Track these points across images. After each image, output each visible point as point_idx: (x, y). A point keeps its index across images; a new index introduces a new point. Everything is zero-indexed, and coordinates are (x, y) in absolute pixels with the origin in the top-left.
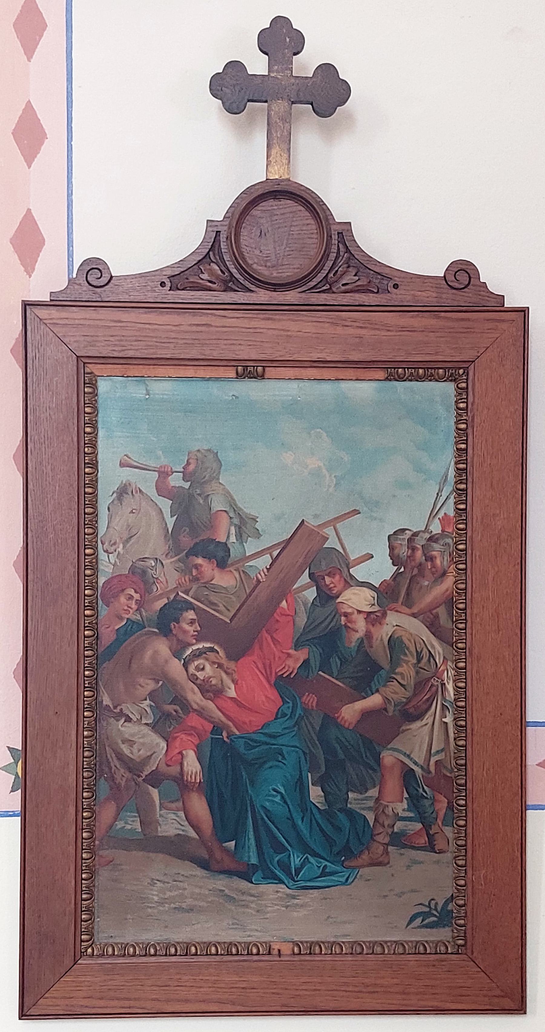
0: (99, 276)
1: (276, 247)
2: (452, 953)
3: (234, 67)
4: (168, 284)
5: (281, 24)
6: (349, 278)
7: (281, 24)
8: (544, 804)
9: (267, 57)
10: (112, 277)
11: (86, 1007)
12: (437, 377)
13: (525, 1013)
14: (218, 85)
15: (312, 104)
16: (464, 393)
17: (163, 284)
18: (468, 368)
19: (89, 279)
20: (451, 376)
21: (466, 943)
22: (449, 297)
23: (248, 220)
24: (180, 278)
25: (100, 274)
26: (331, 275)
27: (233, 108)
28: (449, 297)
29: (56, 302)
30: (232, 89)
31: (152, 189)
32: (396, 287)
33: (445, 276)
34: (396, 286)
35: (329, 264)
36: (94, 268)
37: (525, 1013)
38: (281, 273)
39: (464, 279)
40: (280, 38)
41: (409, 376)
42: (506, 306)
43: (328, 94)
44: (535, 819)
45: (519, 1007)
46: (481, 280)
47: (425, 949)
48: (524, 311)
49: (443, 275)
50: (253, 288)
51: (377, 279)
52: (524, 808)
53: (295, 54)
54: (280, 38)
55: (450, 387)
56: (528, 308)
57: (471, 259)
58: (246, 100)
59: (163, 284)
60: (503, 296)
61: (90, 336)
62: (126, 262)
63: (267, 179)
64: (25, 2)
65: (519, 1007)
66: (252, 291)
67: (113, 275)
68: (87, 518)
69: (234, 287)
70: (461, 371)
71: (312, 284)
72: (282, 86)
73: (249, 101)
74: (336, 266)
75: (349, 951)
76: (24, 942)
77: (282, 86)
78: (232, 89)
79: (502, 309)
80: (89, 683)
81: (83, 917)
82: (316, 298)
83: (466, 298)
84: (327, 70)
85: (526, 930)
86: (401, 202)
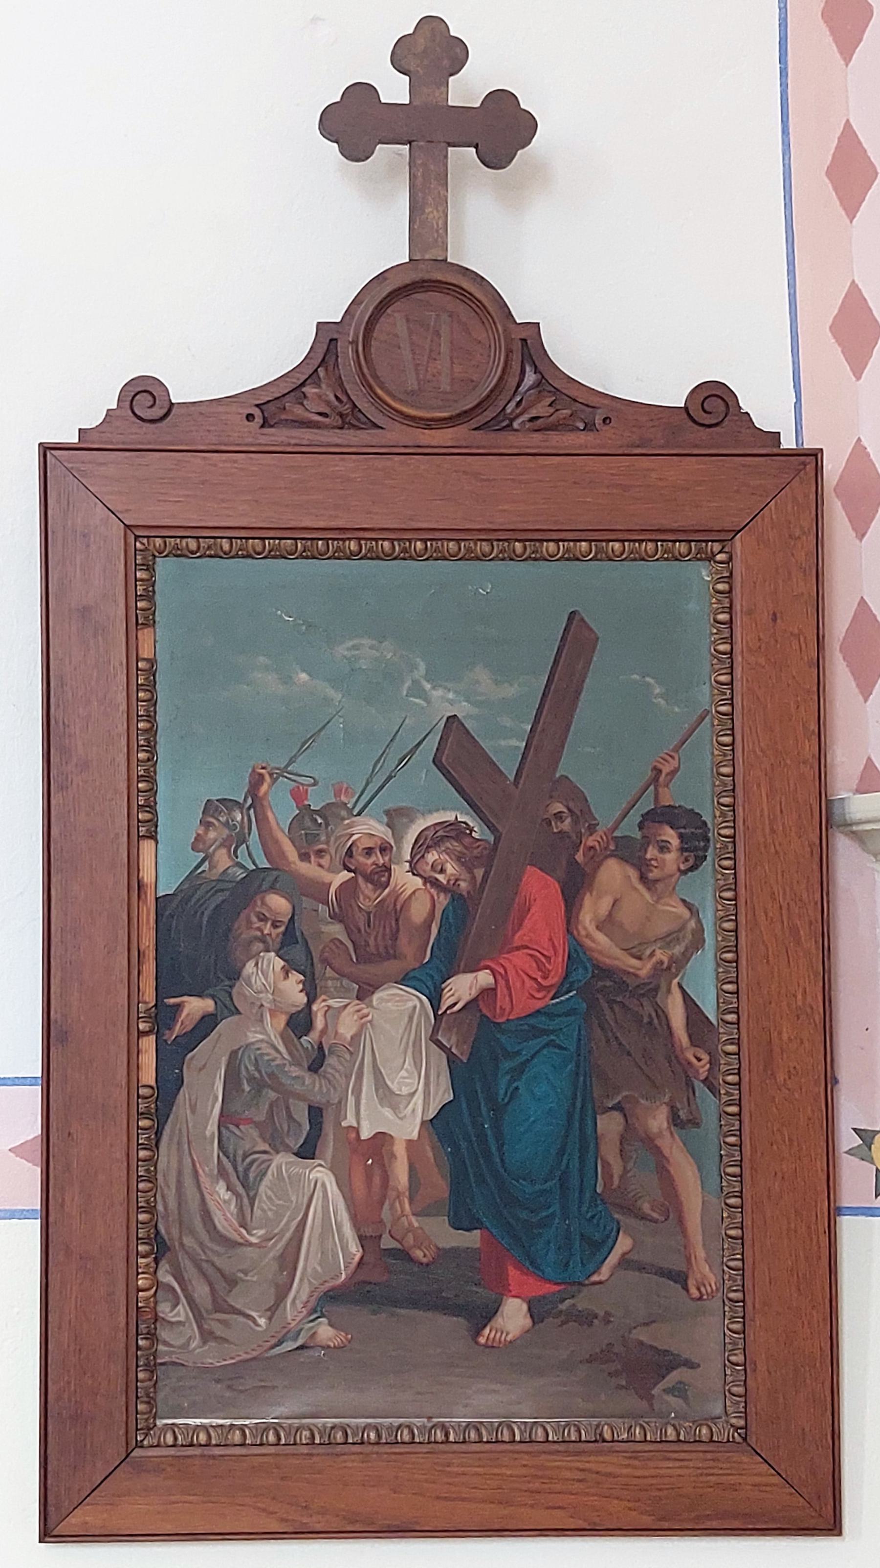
1: (430, 362)
2: (488, 1442)
3: (361, 94)
5: (432, 25)
7: (432, 25)
8: (879, 1206)
10: (172, 404)
12: (447, 554)
13: (840, 1534)
15: (476, 147)
20: (501, 552)
24: (270, 407)
25: (150, 398)
26: (513, 404)
27: (355, 150)
29: (88, 442)
30: (353, 122)
31: (255, 272)
32: (251, 419)
34: (250, 417)
36: (144, 398)
37: (840, 1534)
38: (431, 384)
40: (431, 50)
41: (335, 552)
43: (502, 130)
45: (831, 1525)
47: (480, 1435)
48: (816, 455)
49: (683, 405)
52: (834, 1212)
53: (451, 75)
54: (431, 50)
55: (164, 567)
56: (821, 450)
57: (155, 373)
62: (188, 384)
63: (410, 260)
64: (826, 2)
65: (831, 1525)
66: (376, 426)
67: (173, 401)
69: (354, 422)
71: (489, 414)
72: (432, 120)
75: (358, 1439)
77: (432, 120)
78: (353, 122)
79: (775, 451)
84: (502, 102)
86: (644, 279)
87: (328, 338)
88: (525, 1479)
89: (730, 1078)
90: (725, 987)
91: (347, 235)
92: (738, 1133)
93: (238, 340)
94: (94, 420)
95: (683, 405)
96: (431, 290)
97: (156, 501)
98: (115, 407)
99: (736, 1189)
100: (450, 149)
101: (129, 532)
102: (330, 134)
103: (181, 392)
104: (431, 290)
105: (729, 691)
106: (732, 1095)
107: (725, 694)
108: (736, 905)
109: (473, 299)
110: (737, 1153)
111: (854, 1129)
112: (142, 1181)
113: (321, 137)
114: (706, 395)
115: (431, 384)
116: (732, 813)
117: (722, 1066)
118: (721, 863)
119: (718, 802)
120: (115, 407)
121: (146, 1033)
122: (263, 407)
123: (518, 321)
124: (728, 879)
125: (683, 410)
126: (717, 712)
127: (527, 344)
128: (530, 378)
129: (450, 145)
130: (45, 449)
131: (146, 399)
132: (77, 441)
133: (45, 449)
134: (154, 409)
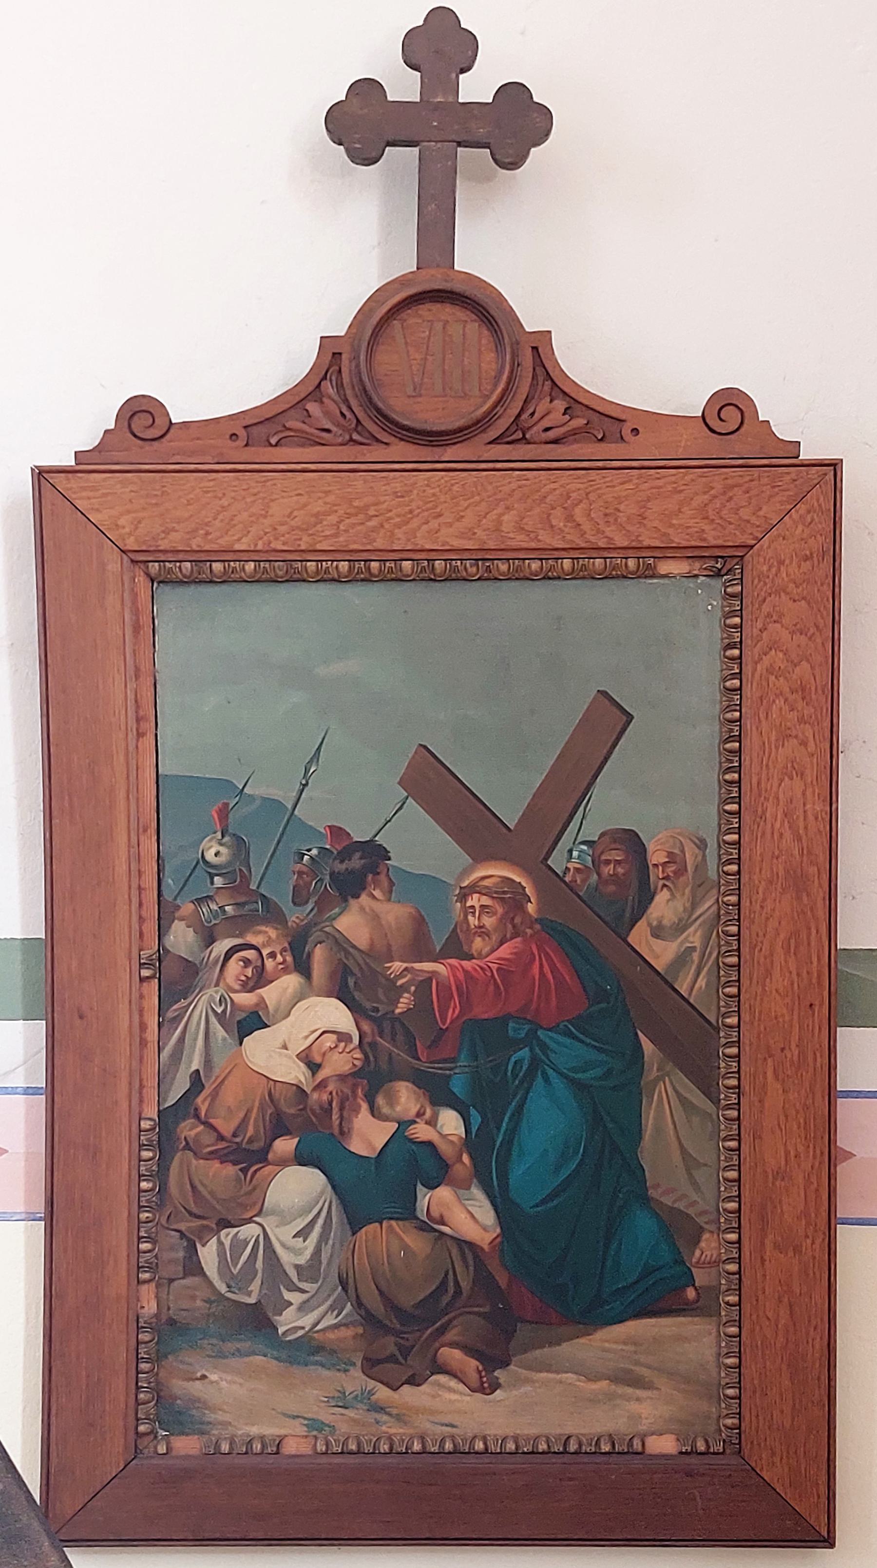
0: (151, 421)
1: (436, 377)
4: (242, 433)
5: (442, 20)
7: (442, 20)
9: (491, 101)
11: (138, 799)
17: (635, 431)
18: (742, 557)
19: (133, 426)
22: (714, 446)
24: (262, 431)
26: (525, 416)
28: (714, 446)
31: (253, 287)
33: (703, 416)
36: (141, 417)
37: (832, 1545)
38: (436, 393)
39: (732, 417)
40: (441, 44)
43: (516, 125)
50: (385, 438)
51: (603, 423)
53: (463, 71)
54: (441, 44)
56: (842, 460)
58: (383, 144)
59: (635, 431)
61: (140, 516)
62: (209, 388)
63: (418, 268)
67: (173, 421)
72: (437, 123)
73: (389, 144)
74: (529, 403)
76: (50, 1341)
77: (437, 123)
78: (361, 125)
83: (738, 446)
84: (514, 94)
86: (627, 293)
87: (331, 352)
89: (729, 1051)
90: (727, 807)
91: (338, 253)
92: (737, 1138)
93: (238, 356)
94: (89, 440)
96: (435, 296)
98: (112, 427)
99: (734, 978)
100: (459, 149)
101: (124, 556)
103: (180, 411)
104: (435, 296)
105: (735, 1064)
106: (731, 854)
109: (480, 306)
110: (736, 1157)
112: (144, 1180)
113: (454, 10)
114: (718, 407)
115: (436, 393)
116: (736, 942)
117: (722, 1039)
122: (249, 429)
123: (527, 330)
127: (533, 357)
129: (459, 144)
130: (41, 475)
131: (147, 420)
132: (73, 463)
133: (41, 475)
134: (151, 430)
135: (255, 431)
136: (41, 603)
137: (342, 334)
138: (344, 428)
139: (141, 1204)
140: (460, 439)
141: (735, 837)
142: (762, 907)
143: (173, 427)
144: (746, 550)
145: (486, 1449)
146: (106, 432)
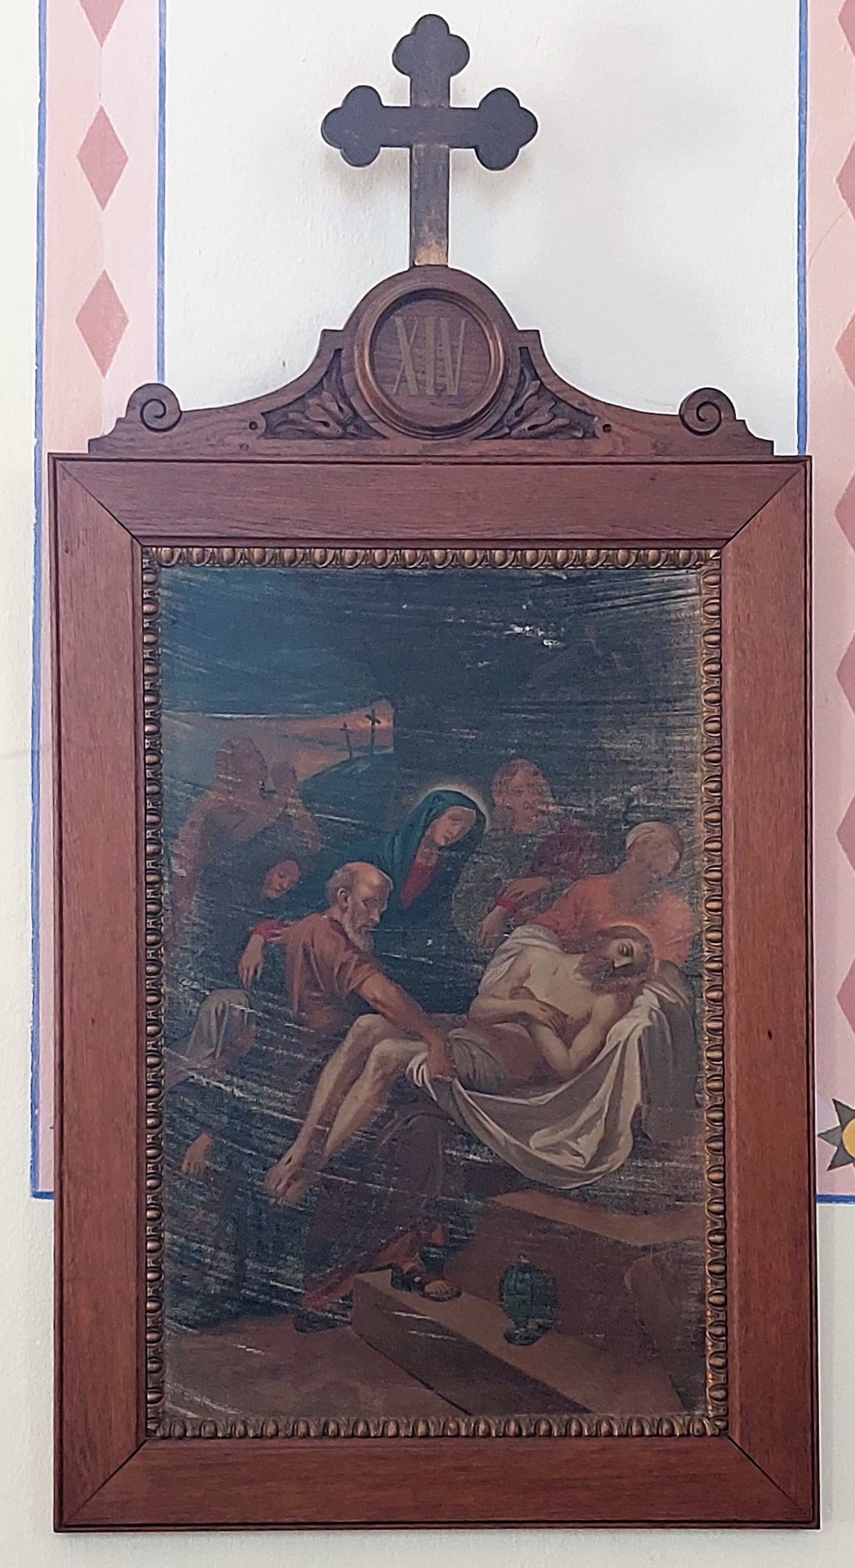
0: (162, 412)
1: (430, 369)
3: (362, 96)
4: (262, 423)
5: (431, 27)
6: (541, 418)
7: (431, 27)
8: (854, 1194)
10: (181, 412)
14: (335, 127)
16: (719, 1098)
21: (721, 668)
23: (381, 349)
24: (277, 415)
27: (359, 156)
31: (255, 292)
32: (253, 426)
33: (681, 416)
35: (509, 395)
36: (153, 405)
40: (431, 49)
42: (776, 454)
43: (503, 130)
44: (835, 1225)
46: (738, 418)
49: (677, 413)
51: (580, 417)
53: (452, 75)
54: (431, 49)
59: (607, 428)
60: (772, 442)
63: (413, 266)
67: (182, 409)
68: (150, 1317)
70: (712, 553)
72: (432, 121)
74: (516, 391)
77: (432, 121)
78: (356, 128)
79: (767, 458)
80: (153, 923)
81: (148, 1305)
82: (485, 446)
84: (501, 99)
85: (738, 1528)
87: (334, 348)
88: (142, 521)
91: (341, 247)
95: (677, 413)
96: (432, 300)
97: (172, 533)
98: (124, 416)
102: (331, 139)
103: (189, 400)
104: (432, 300)
107: (714, 832)
108: (721, 736)
111: (835, 1102)
118: (706, 608)
119: (705, 729)
120: (124, 416)
121: (220, 1117)
122: (267, 415)
123: (519, 328)
124: (714, 802)
125: (679, 418)
126: (710, 1180)
127: (527, 350)
128: (531, 387)
132: (87, 452)
134: (160, 420)
135: (275, 419)
136: (58, 975)
137: (341, 328)
138: (339, 423)
139: (148, 927)
140: (397, 428)
141: (720, 1144)
142: (228, 518)
143: (184, 414)
144: (725, 542)
145: (535, 1433)
146: (119, 420)
